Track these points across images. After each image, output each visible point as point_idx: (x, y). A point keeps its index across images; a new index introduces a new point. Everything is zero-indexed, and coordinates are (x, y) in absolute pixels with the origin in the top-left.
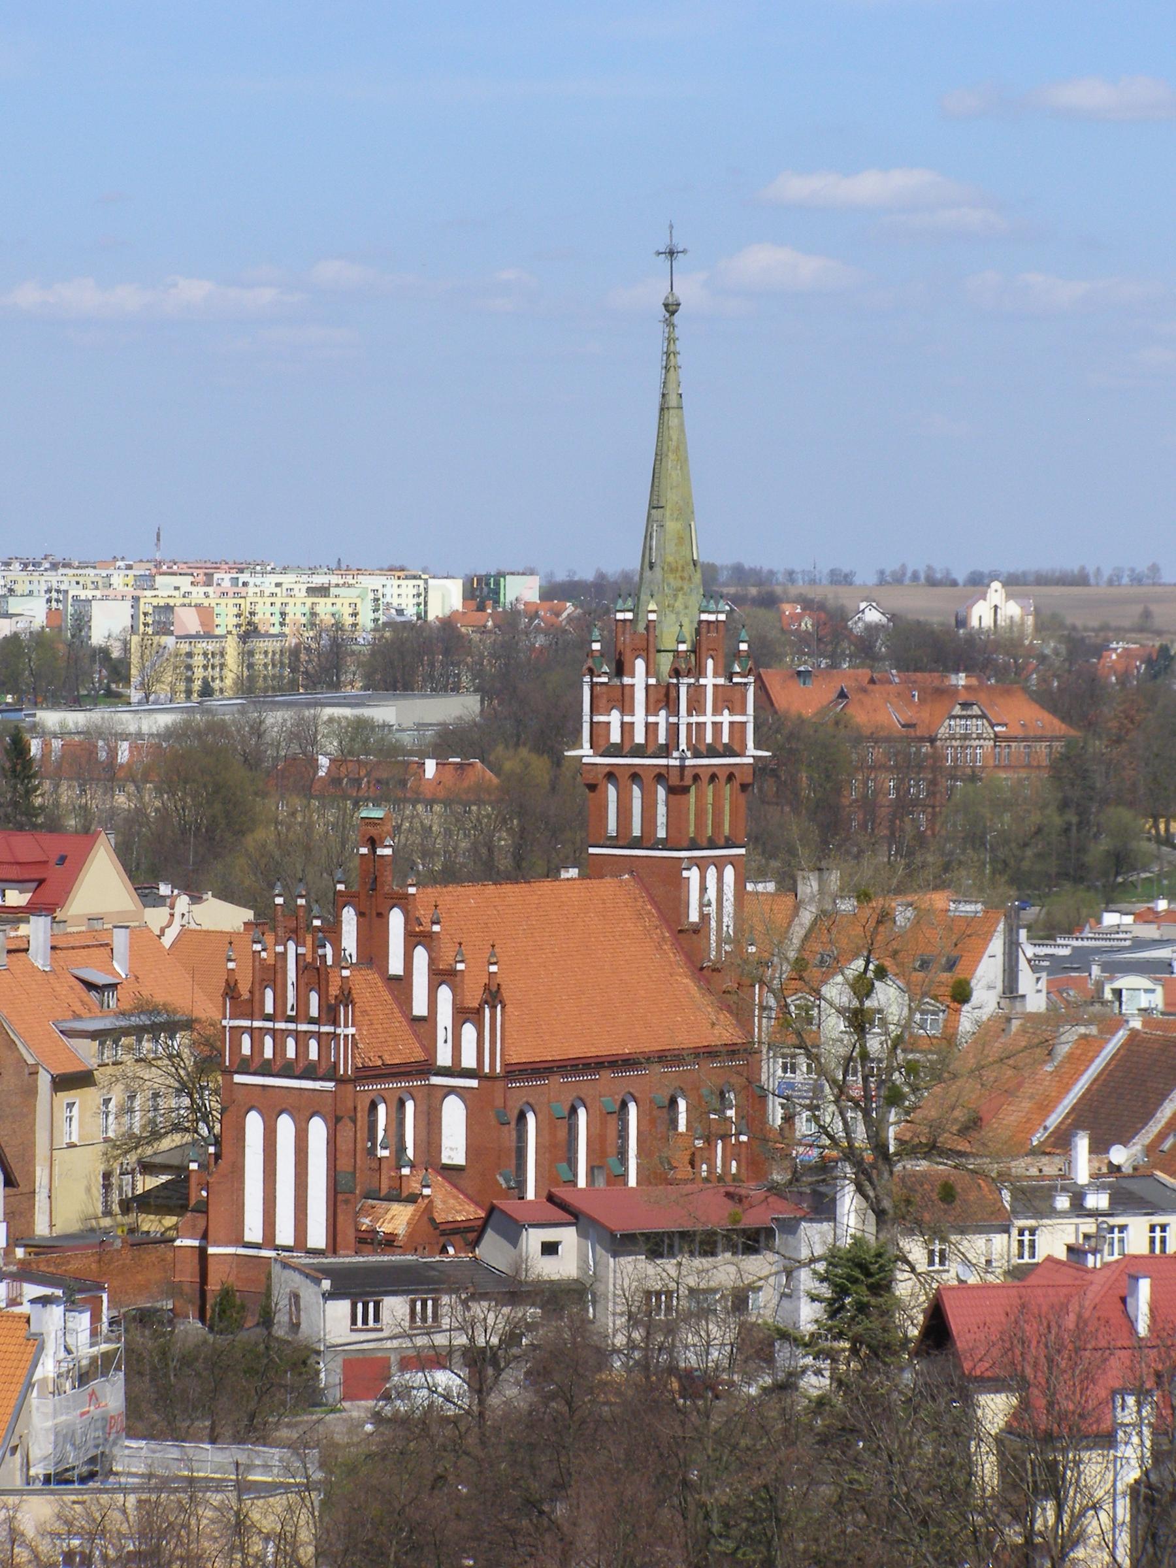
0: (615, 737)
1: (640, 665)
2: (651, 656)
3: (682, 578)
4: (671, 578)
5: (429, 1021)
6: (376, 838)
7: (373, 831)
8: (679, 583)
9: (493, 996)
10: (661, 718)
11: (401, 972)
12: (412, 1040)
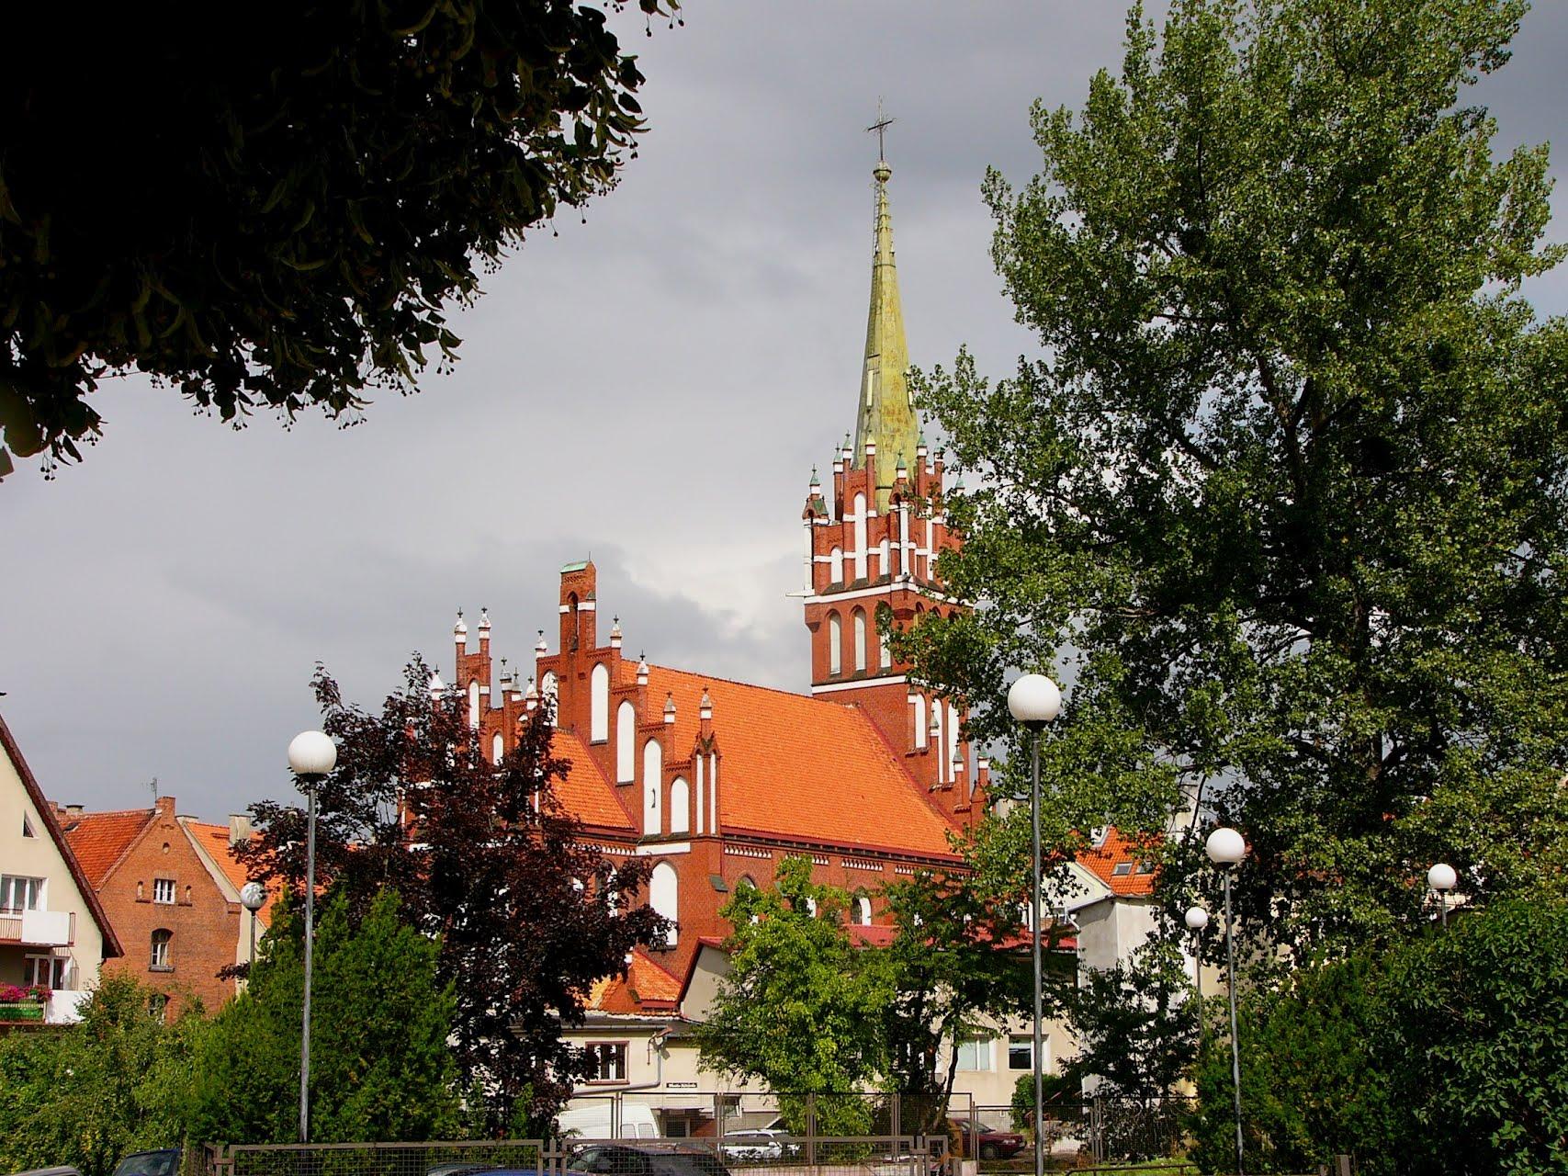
0: (837, 577)
1: (860, 501)
2: (871, 494)
3: (899, 421)
4: (887, 419)
5: (636, 785)
6: (577, 592)
7: (574, 586)
8: (896, 425)
9: (707, 746)
10: (883, 549)
11: (605, 737)
12: (616, 806)
